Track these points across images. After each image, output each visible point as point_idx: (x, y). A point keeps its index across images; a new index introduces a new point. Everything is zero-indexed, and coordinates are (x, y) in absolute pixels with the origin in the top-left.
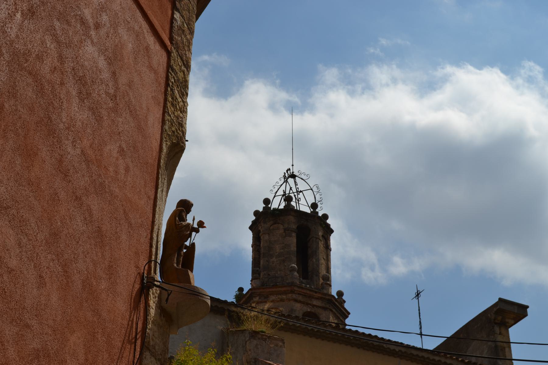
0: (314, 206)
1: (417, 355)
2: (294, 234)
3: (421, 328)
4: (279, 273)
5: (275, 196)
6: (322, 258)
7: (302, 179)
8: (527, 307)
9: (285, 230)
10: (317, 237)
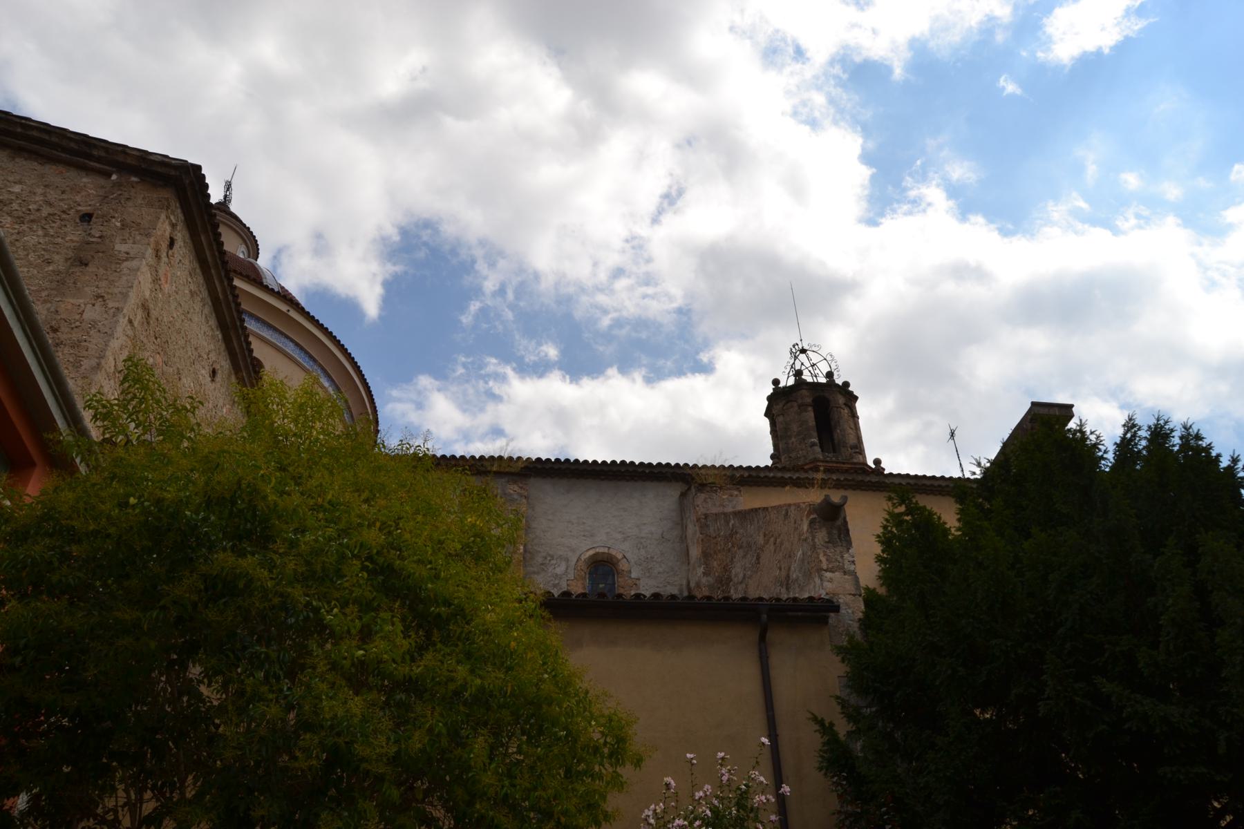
0: (830, 375)
1: (932, 485)
2: (810, 409)
3: (962, 470)
4: (800, 452)
5: (788, 377)
6: (848, 428)
7: (813, 351)
8: (1072, 406)
9: (799, 406)
10: (837, 406)
